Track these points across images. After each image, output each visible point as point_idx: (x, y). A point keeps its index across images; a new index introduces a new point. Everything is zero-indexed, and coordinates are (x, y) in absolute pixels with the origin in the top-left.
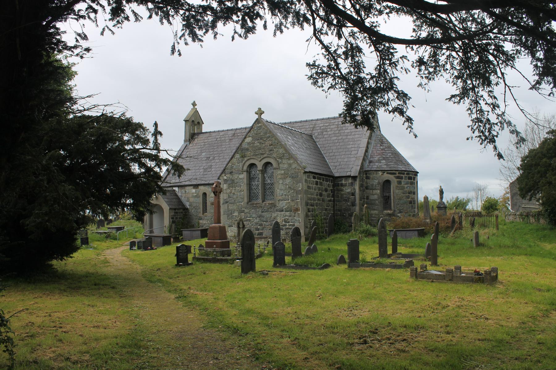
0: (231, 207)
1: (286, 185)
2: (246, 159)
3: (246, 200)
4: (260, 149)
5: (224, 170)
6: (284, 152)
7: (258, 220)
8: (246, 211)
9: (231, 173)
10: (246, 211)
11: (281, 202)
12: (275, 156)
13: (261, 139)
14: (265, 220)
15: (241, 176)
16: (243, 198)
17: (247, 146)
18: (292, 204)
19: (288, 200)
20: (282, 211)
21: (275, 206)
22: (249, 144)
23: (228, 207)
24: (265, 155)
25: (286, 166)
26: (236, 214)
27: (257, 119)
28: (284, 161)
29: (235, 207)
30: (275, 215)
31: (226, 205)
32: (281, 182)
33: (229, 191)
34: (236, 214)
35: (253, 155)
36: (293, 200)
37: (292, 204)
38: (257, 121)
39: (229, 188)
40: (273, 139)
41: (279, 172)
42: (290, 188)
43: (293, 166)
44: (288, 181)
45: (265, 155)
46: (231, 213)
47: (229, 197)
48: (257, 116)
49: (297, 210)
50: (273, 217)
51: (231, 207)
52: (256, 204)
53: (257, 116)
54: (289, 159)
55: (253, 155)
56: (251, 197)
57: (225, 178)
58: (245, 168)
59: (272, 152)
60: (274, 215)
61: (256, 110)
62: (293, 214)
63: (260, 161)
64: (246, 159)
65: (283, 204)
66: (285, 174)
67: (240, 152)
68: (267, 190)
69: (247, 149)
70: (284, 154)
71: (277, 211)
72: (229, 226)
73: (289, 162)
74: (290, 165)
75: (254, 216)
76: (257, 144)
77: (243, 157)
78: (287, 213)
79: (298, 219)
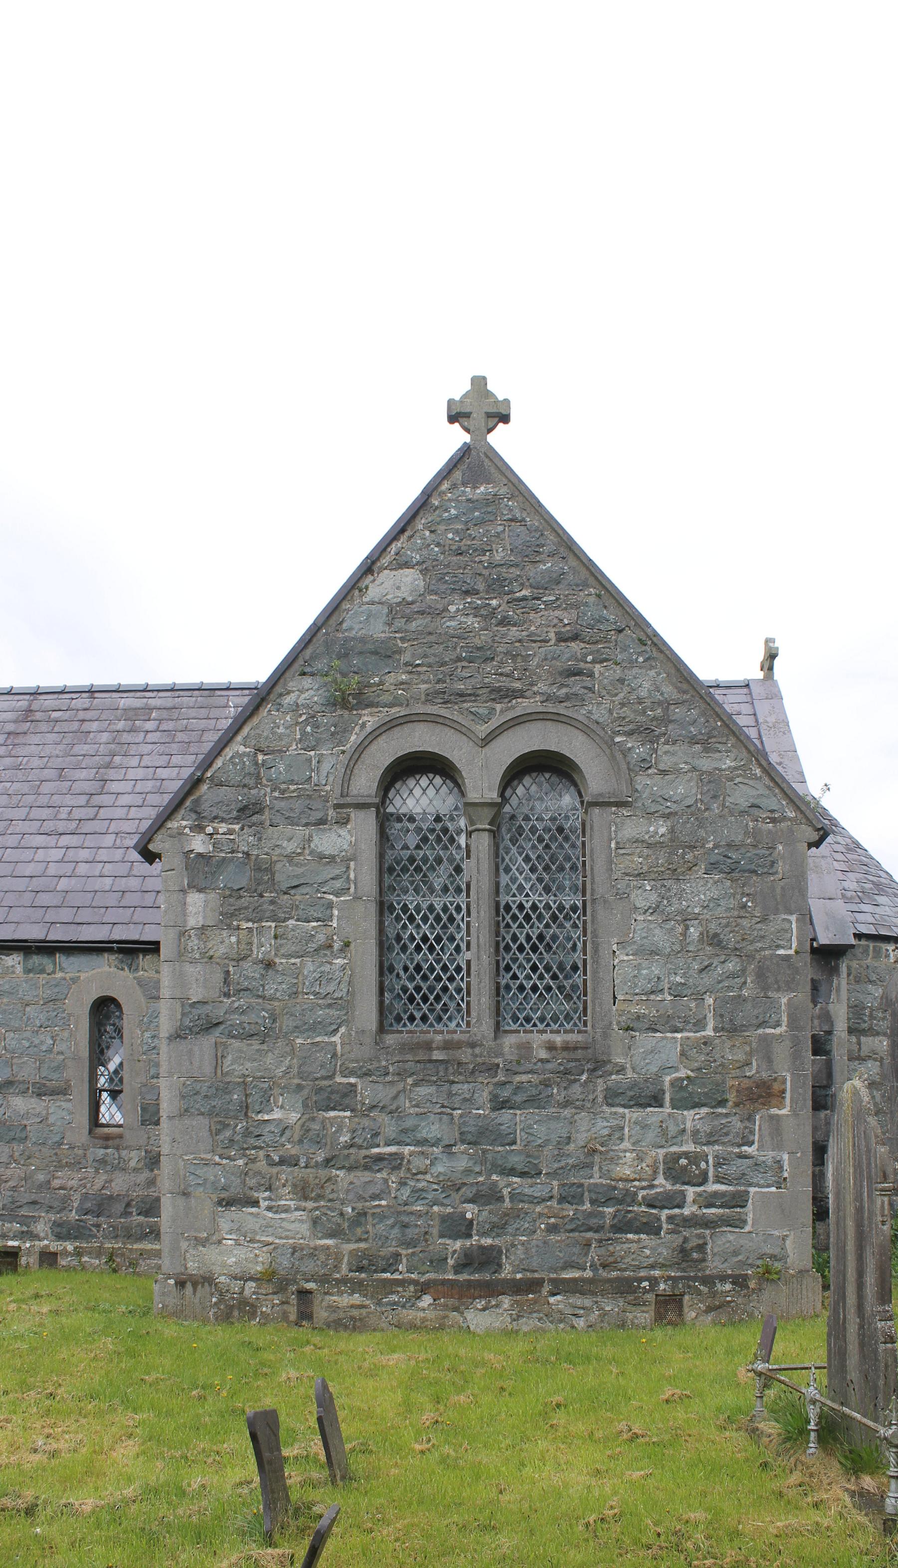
0: (241, 1060)
1: (686, 920)
2: (370, 719)
3: (367, 1013)
4: (483, 655)
5: (195, 783)
6: (669, 691)
7: (462, 1163)
8: (366, 1092)
9: (248, 812)
10: (366, 1092)
11: (645, 1041)
12: (600, 713)
13: (497, 586)
14: (516, 1161)
15: (331, 841)
16: (345, 1005)
17: (378, 630)
18: (732, 1053)
19: (700, 1024)
20: (656, 1100)
21: (599, 1065)
22: (397, 611)
23: (218, 1060)
24: (524, 706)
25: (683, 789)
26: (285, 1113)
27: (465, 451)
28: (671, 755)
29: (275, 1062)
30: (602, 1127)
31: (207, 1042)
32: (644, 895)
33: (225, 943)
34: (285, 1113)
35: (429, 698)
36: (731, 1029)
37: (732, 1053)
38: (473, 465)
39: (227, 918)
40: (589, 594)
41: (632, 828)
42: (714, 940)
43: (741, 795)
44: (702, 892)
45: (524, 706)
46: (245, 1108)
47: (229, 986)
48: (457, 437)
49: (763, 1093)
50: (581, 1138)
51: (241, 1060)
52: (447, 1046)
53: (457, 437)
54: (706, 744)
55: (429, 698)
56: (412, 990)
57: (199, 844)
58: (366, 783)
59: (576, 685)
60: (588, 1128)
61: (459, 389)
62: (737, 1124)
63: (487, 741)
64: (370, 719)
65: (658, 1055)
66: (673, 842)
67: (319, 665)
68: (543, 959)
69: (385, 653)
70: (666, 705)
71: (612, 1097)
72: (228, 1203)
73: (705, 764)
74: (713, 784)
75: (432, 1129)
76: (459, 616)
77: (347, 701)
78: (691, 1118)
79: (769, 1156)
